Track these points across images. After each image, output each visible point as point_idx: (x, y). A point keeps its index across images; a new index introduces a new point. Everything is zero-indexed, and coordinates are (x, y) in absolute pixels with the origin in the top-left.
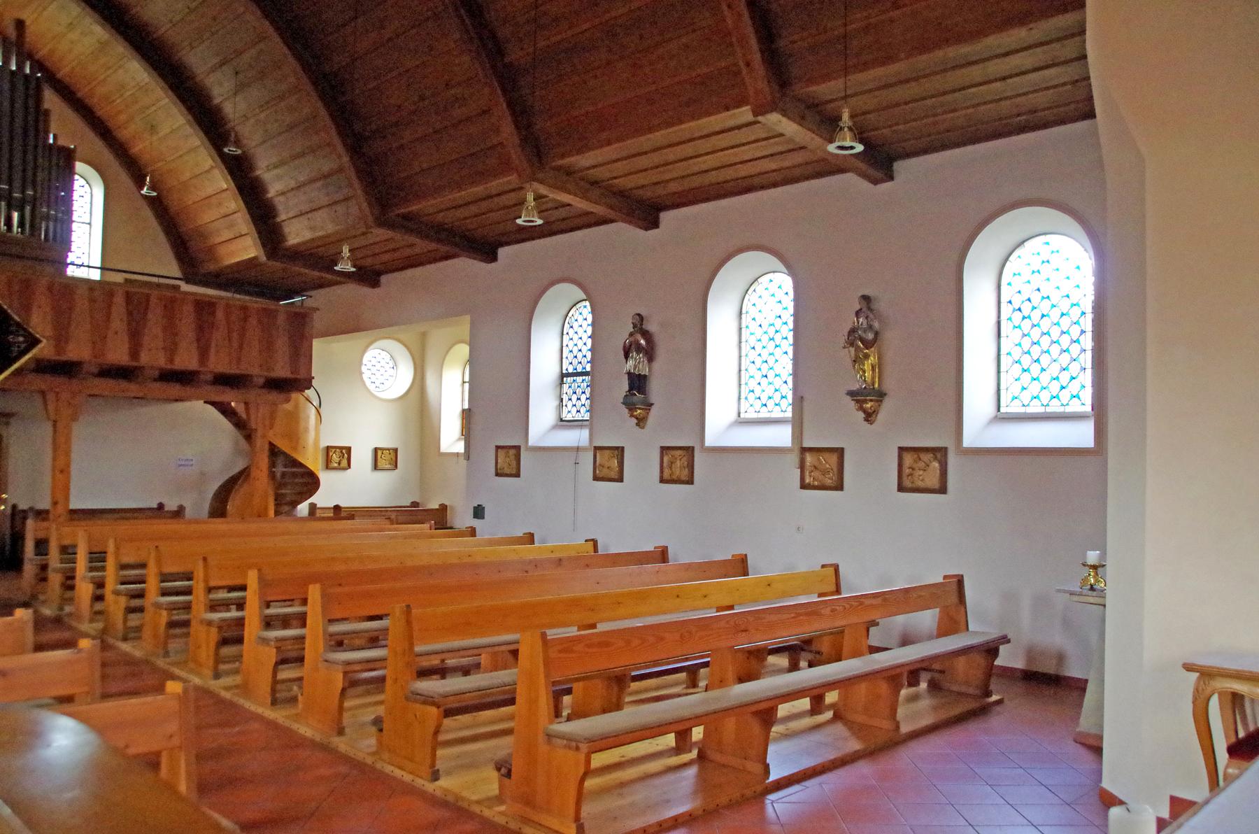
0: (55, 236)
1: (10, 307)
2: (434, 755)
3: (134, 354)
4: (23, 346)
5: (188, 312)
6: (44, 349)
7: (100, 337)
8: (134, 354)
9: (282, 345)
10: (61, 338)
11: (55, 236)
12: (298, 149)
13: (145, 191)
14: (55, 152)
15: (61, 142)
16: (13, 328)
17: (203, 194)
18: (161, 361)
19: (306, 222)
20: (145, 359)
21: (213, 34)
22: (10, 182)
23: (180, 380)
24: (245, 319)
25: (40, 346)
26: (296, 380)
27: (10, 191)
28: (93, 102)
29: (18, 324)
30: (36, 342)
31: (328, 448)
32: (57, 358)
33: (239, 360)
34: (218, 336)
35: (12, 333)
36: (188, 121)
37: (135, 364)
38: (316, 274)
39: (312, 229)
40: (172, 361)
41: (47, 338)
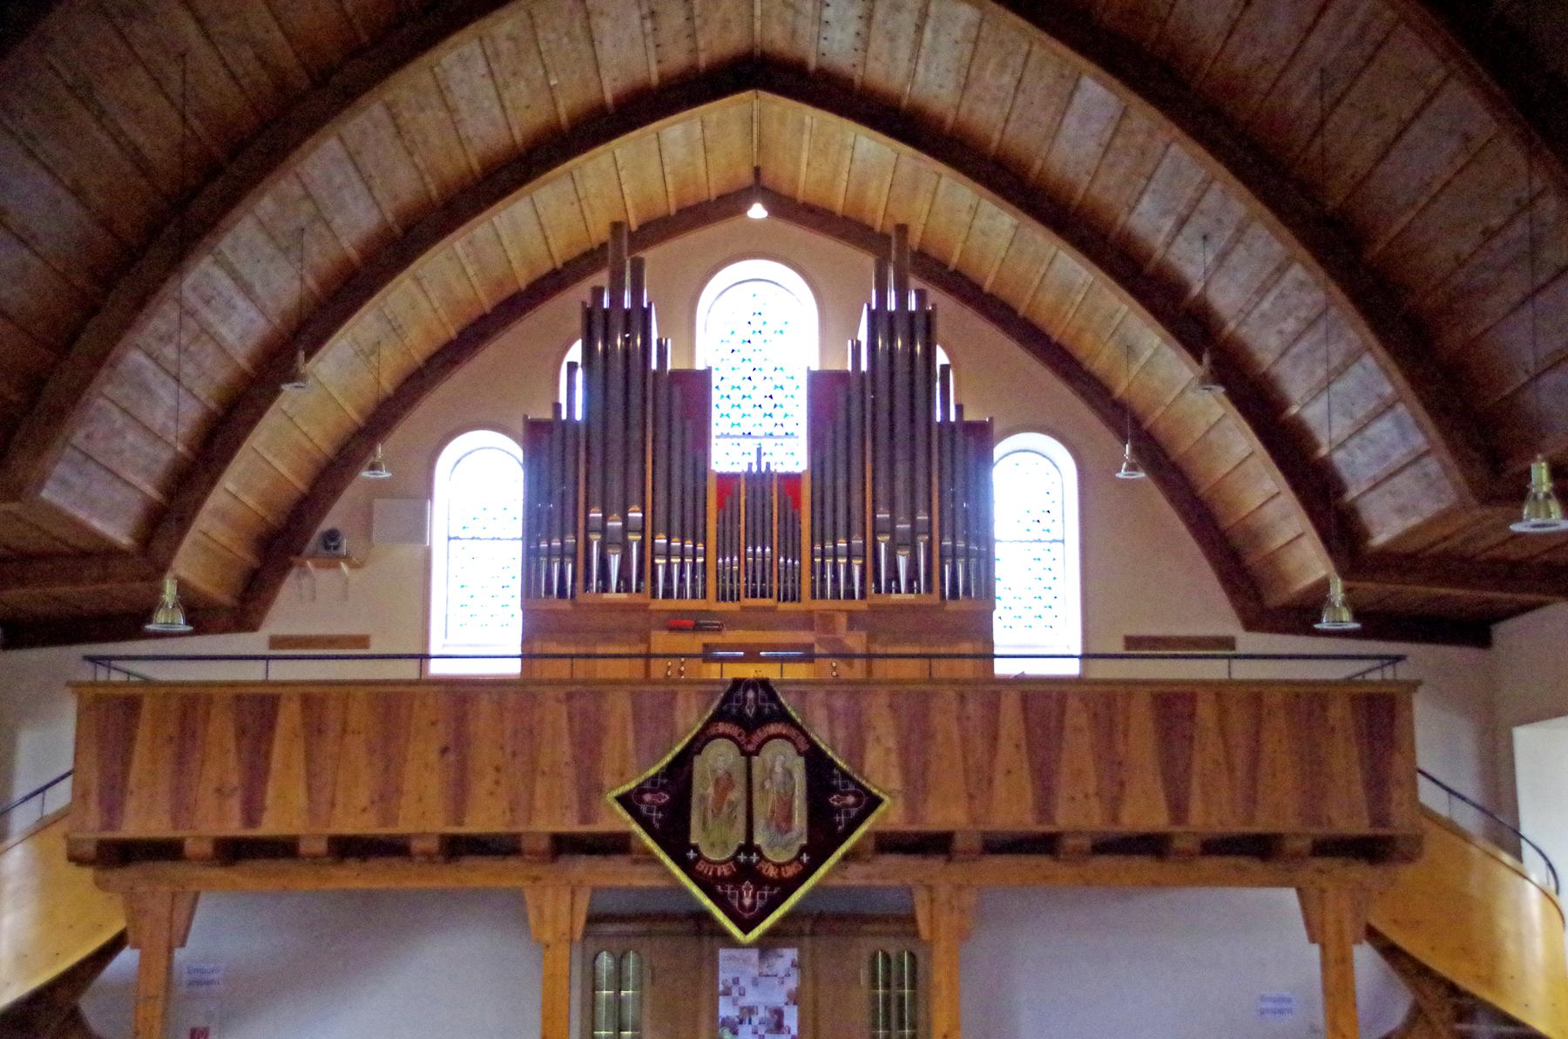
0: (967, 591)
1: (833, 748)
2: (170, 959)
3: (1044, 808)
4: (854, 811)
5: (1141, 718)
6: (890, 815)
7: (980, 784)
8: (1044, 808)
9: (1345, 762)
10: (916, 786)
11: (967, 591)
12: (1336, 361)
13: (1122, 474)
14: (960, 434)
15: (969, 416)
16: (838, 782)
17: (1225, 471)
18: (440, 825)
19: (1389, 500)
20: (1064, 819)
21: (1149, 178)
22: (892, 508)
23: (1255, 851)
24: (1258, 721)
25: (881, 809)
26: (1388, 841)
27: (893, 521)
28: (1041, 318)
29: (845, 775)
30: (875, 802)
31: (905, 922)
32: (914, 828)
33: (1252, 800)
34: (1206, 754)
35: (835, 790)
36: (1165, 340)
37: (1380, 831)
38: (1507, 596)
39: (1401, 510)
40: (1115, 819)
41: (889, 793)
